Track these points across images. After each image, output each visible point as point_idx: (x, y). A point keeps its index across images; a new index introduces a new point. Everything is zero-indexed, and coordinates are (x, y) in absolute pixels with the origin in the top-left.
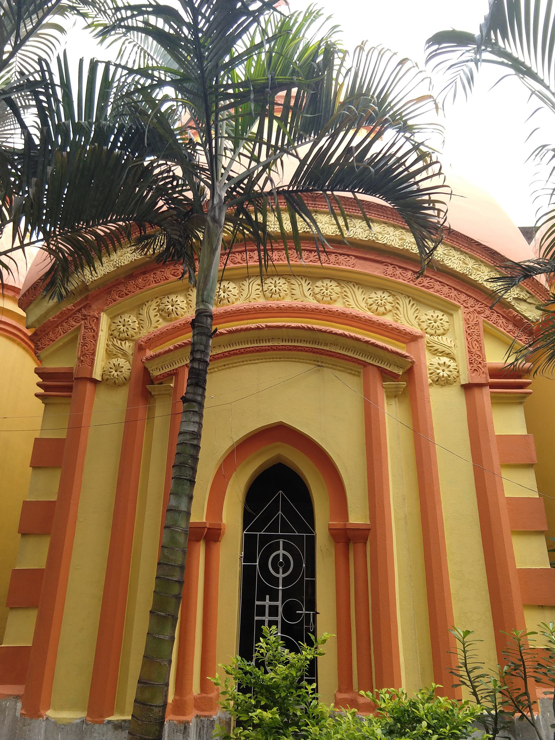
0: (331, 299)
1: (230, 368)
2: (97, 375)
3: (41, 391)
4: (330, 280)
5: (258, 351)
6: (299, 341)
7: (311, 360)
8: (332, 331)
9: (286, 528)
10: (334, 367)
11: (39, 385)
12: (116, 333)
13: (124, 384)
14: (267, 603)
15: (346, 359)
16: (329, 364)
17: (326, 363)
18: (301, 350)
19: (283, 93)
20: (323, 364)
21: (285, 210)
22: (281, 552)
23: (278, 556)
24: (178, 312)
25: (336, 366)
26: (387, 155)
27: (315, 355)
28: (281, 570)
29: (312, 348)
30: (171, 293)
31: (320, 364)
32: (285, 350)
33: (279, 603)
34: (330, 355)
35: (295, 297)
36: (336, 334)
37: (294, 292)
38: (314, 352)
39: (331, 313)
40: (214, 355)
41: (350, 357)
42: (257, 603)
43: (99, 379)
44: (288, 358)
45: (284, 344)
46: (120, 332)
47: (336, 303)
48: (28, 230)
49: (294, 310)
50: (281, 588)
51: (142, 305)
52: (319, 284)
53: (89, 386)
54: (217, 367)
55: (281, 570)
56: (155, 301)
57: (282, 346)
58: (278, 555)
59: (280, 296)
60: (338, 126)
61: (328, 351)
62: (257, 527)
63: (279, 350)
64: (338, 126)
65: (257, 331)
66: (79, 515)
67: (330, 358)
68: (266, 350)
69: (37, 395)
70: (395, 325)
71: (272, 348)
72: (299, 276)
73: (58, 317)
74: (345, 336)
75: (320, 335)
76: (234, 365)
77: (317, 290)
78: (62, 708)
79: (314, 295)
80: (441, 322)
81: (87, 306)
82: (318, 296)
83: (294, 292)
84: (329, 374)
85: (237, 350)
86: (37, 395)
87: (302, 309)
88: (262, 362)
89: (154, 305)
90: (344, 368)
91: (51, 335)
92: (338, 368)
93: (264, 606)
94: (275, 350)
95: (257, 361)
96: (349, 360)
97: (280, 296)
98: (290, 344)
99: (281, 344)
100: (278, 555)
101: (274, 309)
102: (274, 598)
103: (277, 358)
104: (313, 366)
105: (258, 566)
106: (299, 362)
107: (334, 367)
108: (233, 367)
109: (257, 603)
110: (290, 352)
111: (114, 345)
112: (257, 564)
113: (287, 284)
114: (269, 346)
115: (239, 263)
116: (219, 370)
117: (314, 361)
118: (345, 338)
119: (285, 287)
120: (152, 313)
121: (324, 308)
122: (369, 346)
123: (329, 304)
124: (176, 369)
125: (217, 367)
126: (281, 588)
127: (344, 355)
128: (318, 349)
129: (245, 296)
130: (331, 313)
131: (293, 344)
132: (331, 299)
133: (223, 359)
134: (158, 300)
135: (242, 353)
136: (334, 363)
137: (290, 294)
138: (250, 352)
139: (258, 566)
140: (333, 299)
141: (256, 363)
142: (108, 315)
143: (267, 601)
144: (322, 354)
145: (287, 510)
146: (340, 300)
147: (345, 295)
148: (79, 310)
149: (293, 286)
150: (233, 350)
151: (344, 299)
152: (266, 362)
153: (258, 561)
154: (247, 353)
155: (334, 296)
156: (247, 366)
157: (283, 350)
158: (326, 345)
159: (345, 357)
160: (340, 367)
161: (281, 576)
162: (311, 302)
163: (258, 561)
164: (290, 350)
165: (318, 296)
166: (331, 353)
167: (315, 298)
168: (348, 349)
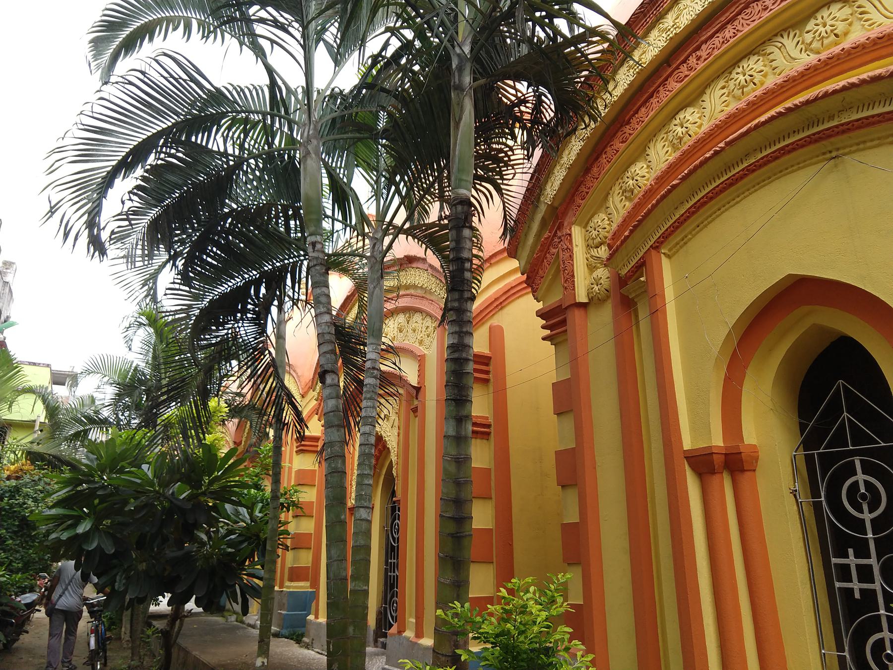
0: (836, 35)
1: (706, 226)
2: (582, 297)
3: (548, 332)
4: (826, 8)
5: (731, 185)
6: (786, 136)
7: (818, 156)
8: (826, 92)
10: (861, 146)
11: (544, 327)
12: (590, 242)
13: (608, 297)
14: (852, 560)
15: (874, 124)
16: (851, 146)
17: (844, 148)
18: (794, 149)
20: (841, 152)
22: (860, 477)
23: (856, 484)
24: (640, 184)
25: (864, 142)
27: (818, 145)
28: (865, 507)
29: (808, 137)
30: (629, 166)
31: (834, 154)
32: (769, 162)
33: (873, 561)
34: (844, 132)
35: (778, 71)
36: (835, 92)
37: (774, 64)
38: (816, 141)
39: (835, 59)
40: (679, 219)
41: (878, 115)
43: (585, 300)
44: (781, 171)
45: (765, 153)
46: (593, 239)
47: (849, 36)
49: (774, 93)
51: (606, 198)
52: (810, 25)
53: (577, 314)
54: (690, 233)
55: (865, 507)
56: (617, 183)
57: (762, 158)
58: (857, 482)
59: (755, 84)
61: (837, 127)
63: (761, 166)
65: (717, 158)
66: (596, 458)
67: (845, 136)
68: (742, 178)
69: (544, 339)
70: (873, 35)
71: (750, 170)
72: (776, 35)
73: (541, 251)
74: (853, 85)
75: (812, 109)
76: (710, 219)
77: (808, 37)
78: (345, 569)
79: (808, 48)
80: (832, 17)
81: (560, 227)
82: (815, 45)
83: (774, 64)
84: (852, 163)
85: (703, 197)
86: (544, 339)
87: (786, 84)
88: (745, 197)
89: (617, 189)
90: (879, 139)
91: (540, 272)
92: (869, 144)
93: (848, 566)
94: (754, 171)
95: (738, 199)
96: (879, 122)
97: (755, 84)
98: (774, 149)
99: (760, 156)
101: (744, 110)
102: (862, 551)
103: (764, 181)
104: (820, 165)
105: (824, 503)
106: (799, 169)
107: (862, 146)
108: (709, 223)
110: (778, 162)
111: (592, 256)
112: (823, 499)
113: (761, 59)
114: (743, 170)
115: (686, 76)
116: (694, 236)
117: (824, 154)
118: (854, 89)
119: (759, 66)
120: (617, 199)
121: (819, 60)
122: (860, 90)
123: (836, 44)
124: (643, 257)
125: (690, 233)
126: (870, 535)
127: (867, 118)
128: (819, 133)
129: (707, 116)
130: (835, 59)
131: (778, 146)
132: (836, 35)
133: (692, 219)
134: (620, 181)
135: (712, 198)
136: (857, 141)
137: (770, 71)
138: (721, 191)
139: (824, 503)
140: (839, 33)
141: (737, 203)
142: (579, 225)
143: (852, 557)
144: (830, 136)
145: (856, 407)
146: (857, 26)
147: (861, 14)
148: (555, 235)
149: (771, 57)
150: (699, 200)
151: (861, 19)
152: (751, 194)
154: (717, 194)
155: (841, 27)
156: (727, 213)
157: (765, 164)
158: (831, 118)
159: (871, 120)
160: (872, 140)
161: (867, 517)
162: (807, 59)
164: (777, 158)
165: (815, 45)
166: (846, 127)
167: (812, 50)
168: (872, 104)
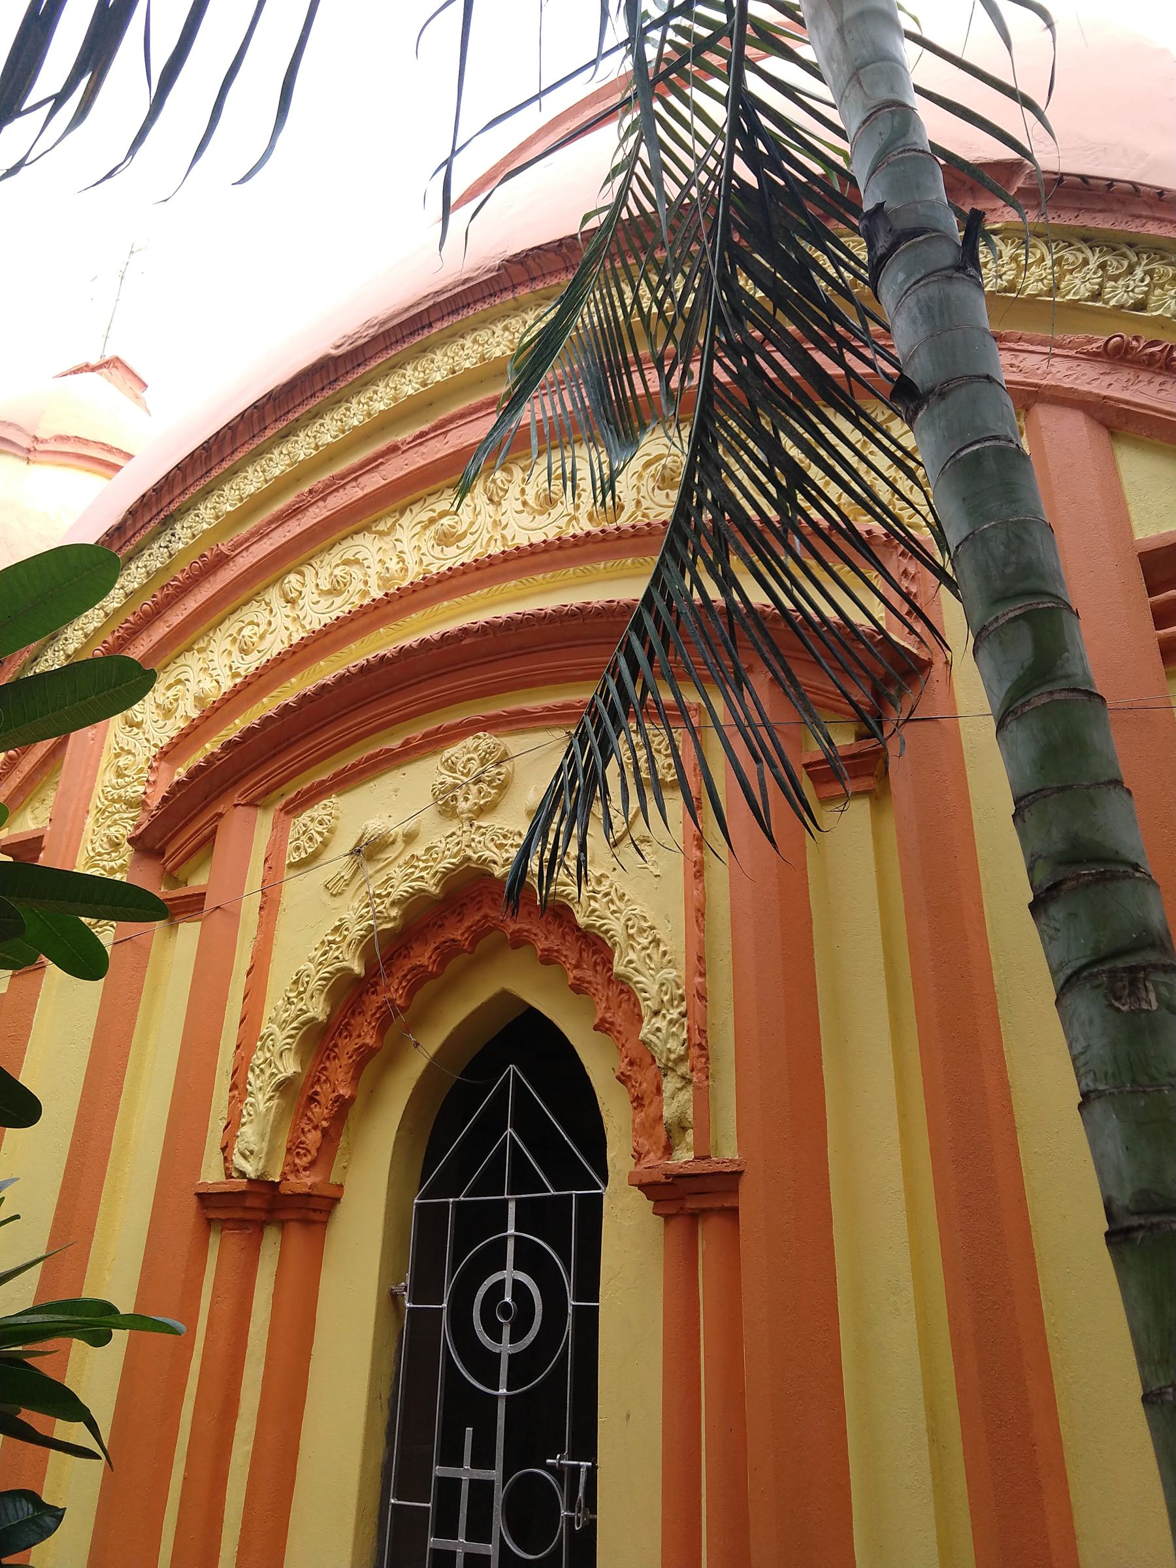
9: (524, 1180)
19: (638, 165)
21: (890, 419)
26: (665, 175)
28: (506, 1332)
33: (495, 1475)
42: (438, 1471)
48: (688, 322)
50: (503, 1391)
55: (506, 1332)
60: (762, 147)
62: (448, 1184)
64: (762, 147)
100: (502, 1283)
109: (438, 1471)
112: (445, 1305)
126: (503, 1391)
145: (530, 1122)
153: (446, 1300)
163: (446, 1300)
